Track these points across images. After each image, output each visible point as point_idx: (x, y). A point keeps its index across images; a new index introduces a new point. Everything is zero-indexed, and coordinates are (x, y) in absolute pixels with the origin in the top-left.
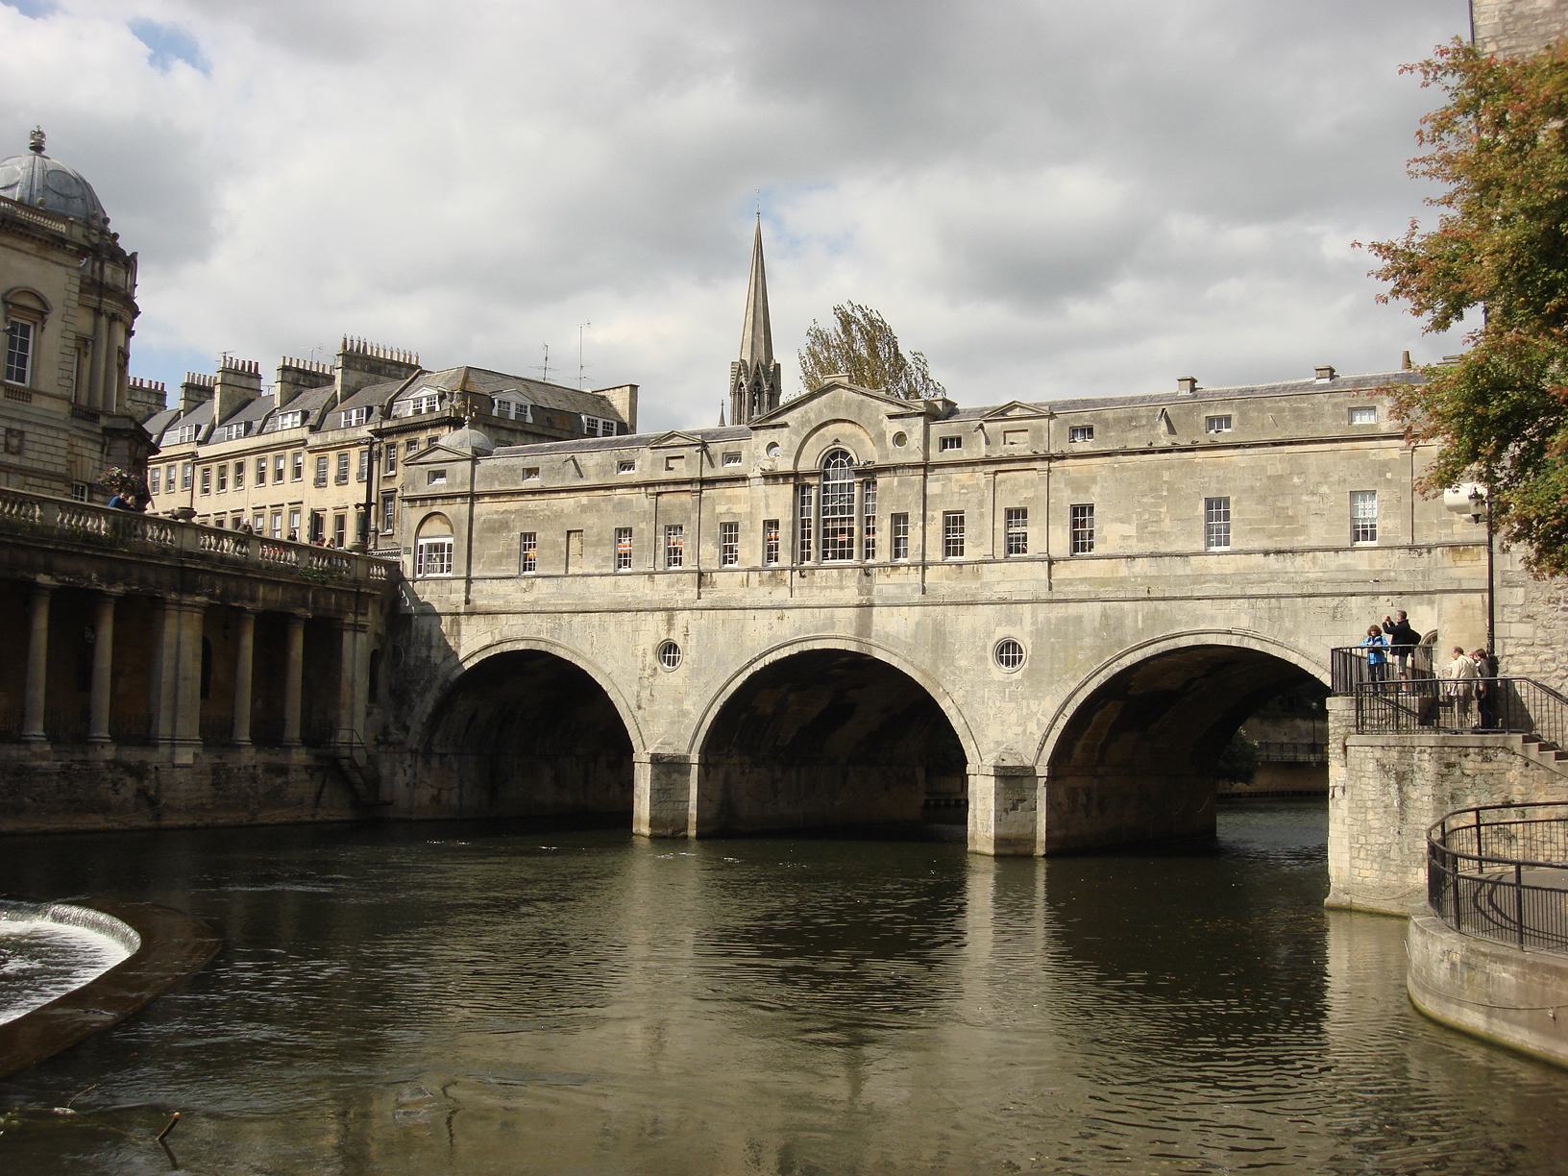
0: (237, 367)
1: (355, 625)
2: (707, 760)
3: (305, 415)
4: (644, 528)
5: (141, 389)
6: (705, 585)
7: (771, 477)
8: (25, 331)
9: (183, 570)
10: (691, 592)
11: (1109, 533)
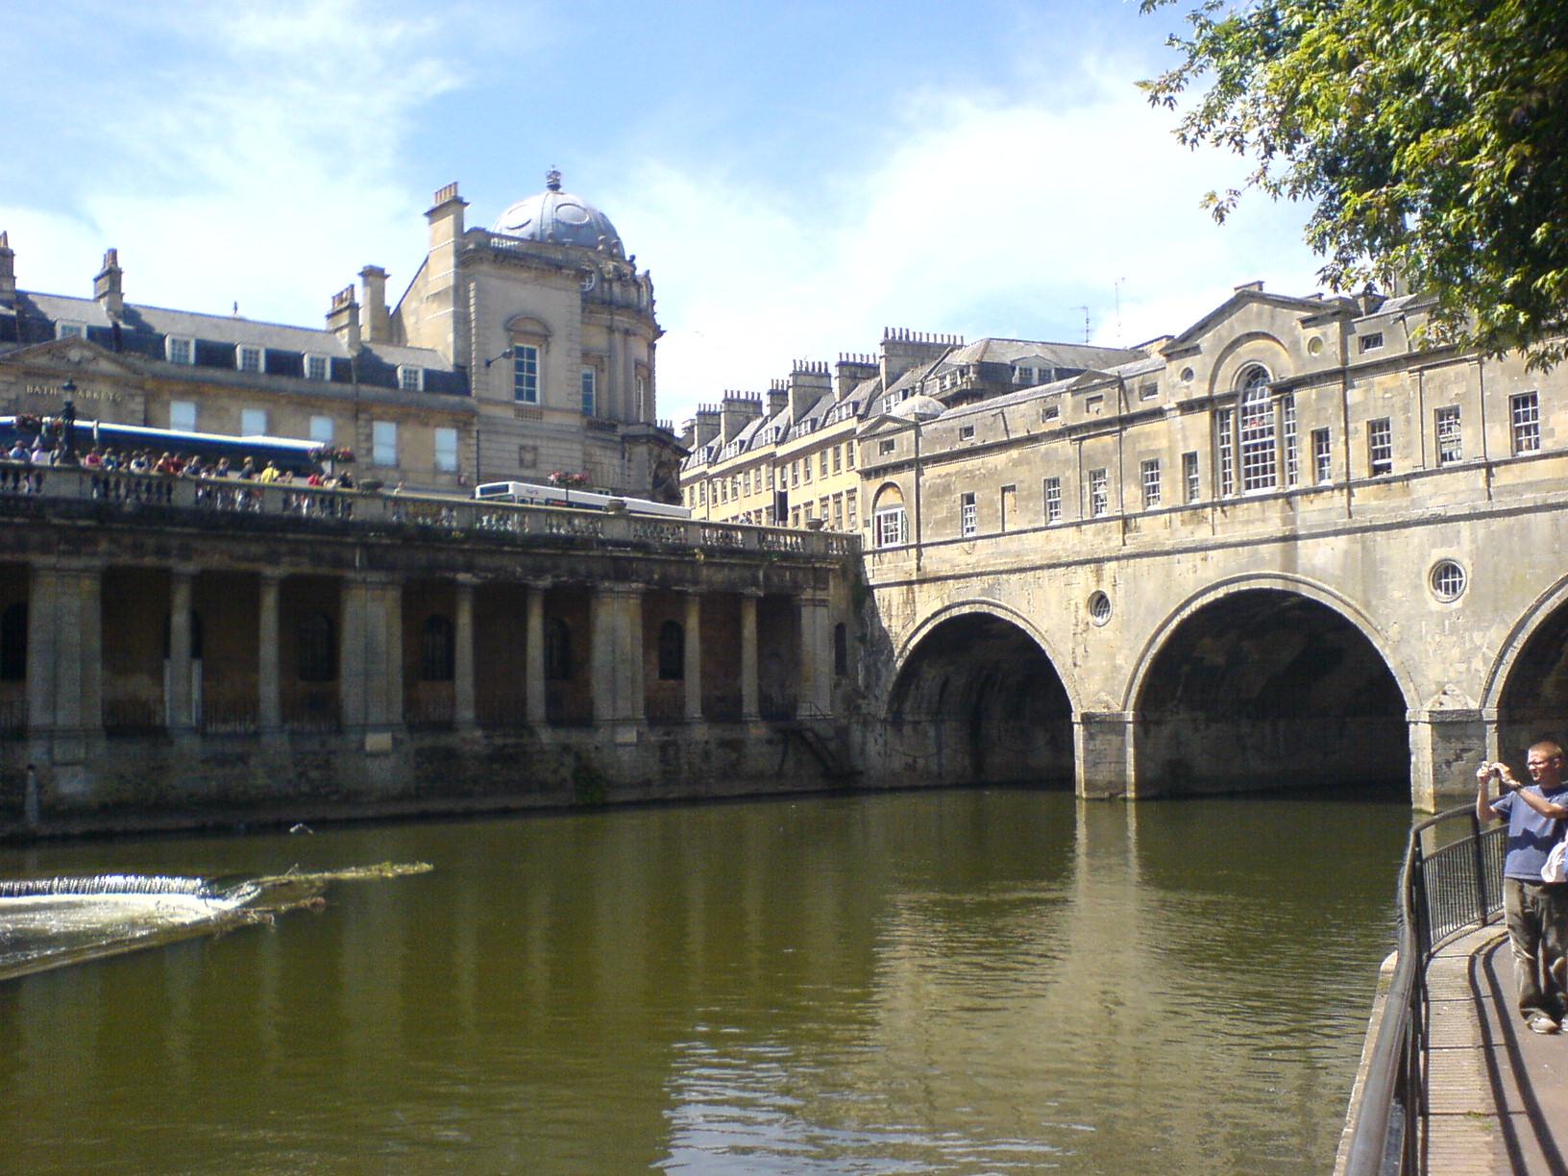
0: (807, 368)
1: (813, 600)
2: (1143, 715)
3: (856, 405)
4: (1070, 476)
5: (739, 400)
6: (1130, 531)
7: (1188, 407)
8: (532, 354)
10: (1116, 539)
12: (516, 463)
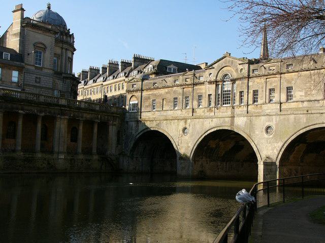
3: (125, 73)
5: (93, 69)
7: (210, 83)
8: (41, 53)
9: (61, 110)
11: (298, 94)
12: (34, 82)
